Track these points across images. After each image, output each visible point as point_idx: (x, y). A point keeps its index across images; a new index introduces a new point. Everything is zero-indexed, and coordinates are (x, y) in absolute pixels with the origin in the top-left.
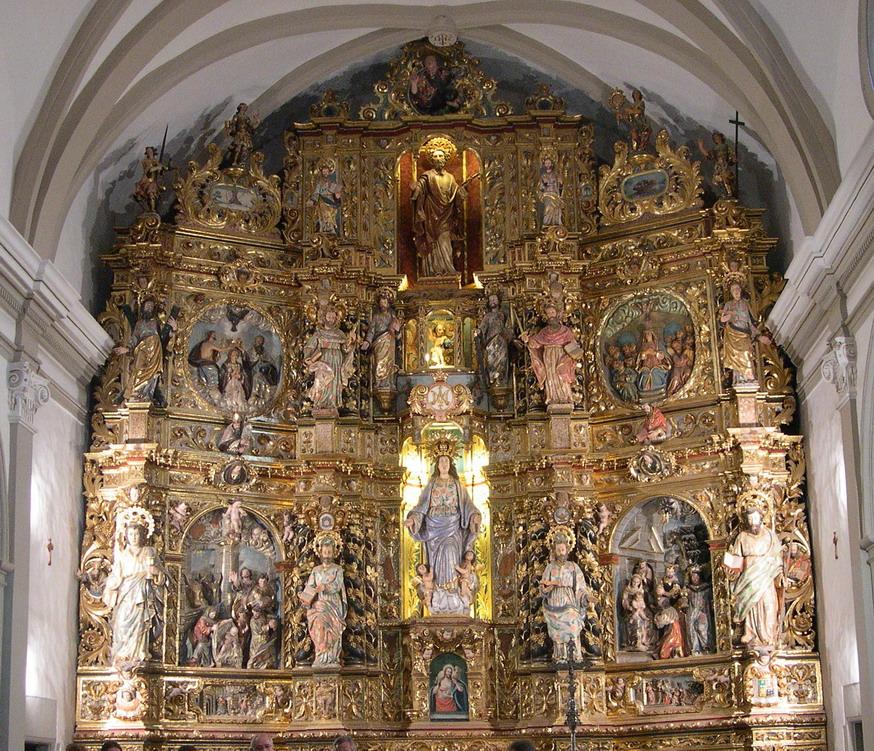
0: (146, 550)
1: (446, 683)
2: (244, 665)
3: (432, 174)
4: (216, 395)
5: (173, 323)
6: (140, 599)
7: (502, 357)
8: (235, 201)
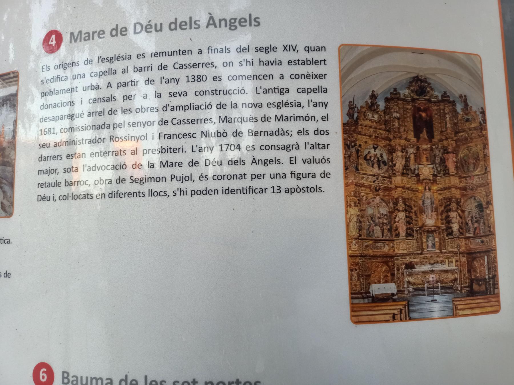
0: (356, 208)
1: (430, 242)
2: (383, 237)
3: (421, 113)
4: (381, 197)
5: (359, 149)
6: (356, 220)
7: (439, 161)
8: (373, 117)
